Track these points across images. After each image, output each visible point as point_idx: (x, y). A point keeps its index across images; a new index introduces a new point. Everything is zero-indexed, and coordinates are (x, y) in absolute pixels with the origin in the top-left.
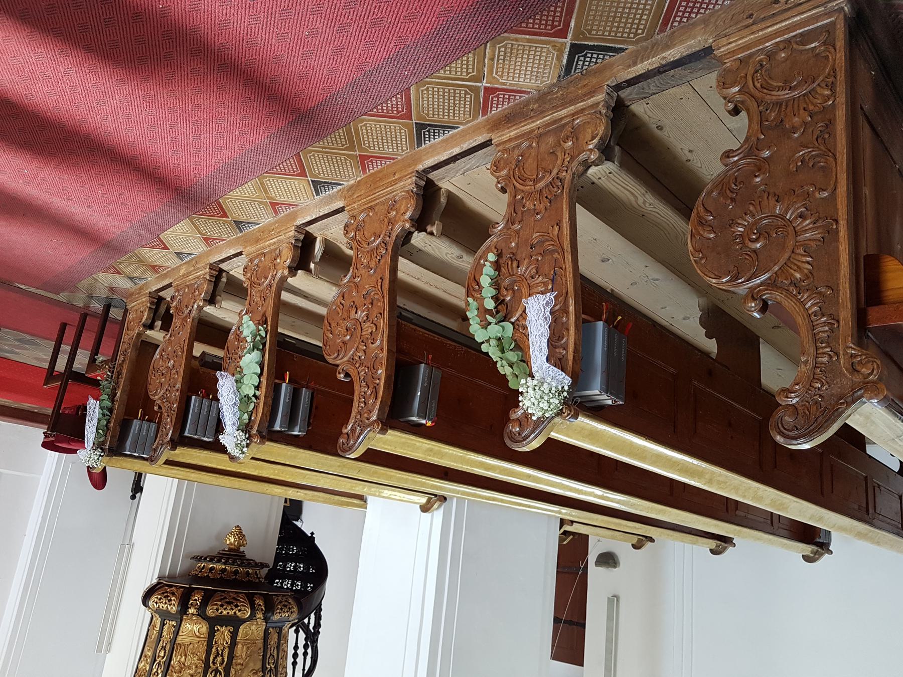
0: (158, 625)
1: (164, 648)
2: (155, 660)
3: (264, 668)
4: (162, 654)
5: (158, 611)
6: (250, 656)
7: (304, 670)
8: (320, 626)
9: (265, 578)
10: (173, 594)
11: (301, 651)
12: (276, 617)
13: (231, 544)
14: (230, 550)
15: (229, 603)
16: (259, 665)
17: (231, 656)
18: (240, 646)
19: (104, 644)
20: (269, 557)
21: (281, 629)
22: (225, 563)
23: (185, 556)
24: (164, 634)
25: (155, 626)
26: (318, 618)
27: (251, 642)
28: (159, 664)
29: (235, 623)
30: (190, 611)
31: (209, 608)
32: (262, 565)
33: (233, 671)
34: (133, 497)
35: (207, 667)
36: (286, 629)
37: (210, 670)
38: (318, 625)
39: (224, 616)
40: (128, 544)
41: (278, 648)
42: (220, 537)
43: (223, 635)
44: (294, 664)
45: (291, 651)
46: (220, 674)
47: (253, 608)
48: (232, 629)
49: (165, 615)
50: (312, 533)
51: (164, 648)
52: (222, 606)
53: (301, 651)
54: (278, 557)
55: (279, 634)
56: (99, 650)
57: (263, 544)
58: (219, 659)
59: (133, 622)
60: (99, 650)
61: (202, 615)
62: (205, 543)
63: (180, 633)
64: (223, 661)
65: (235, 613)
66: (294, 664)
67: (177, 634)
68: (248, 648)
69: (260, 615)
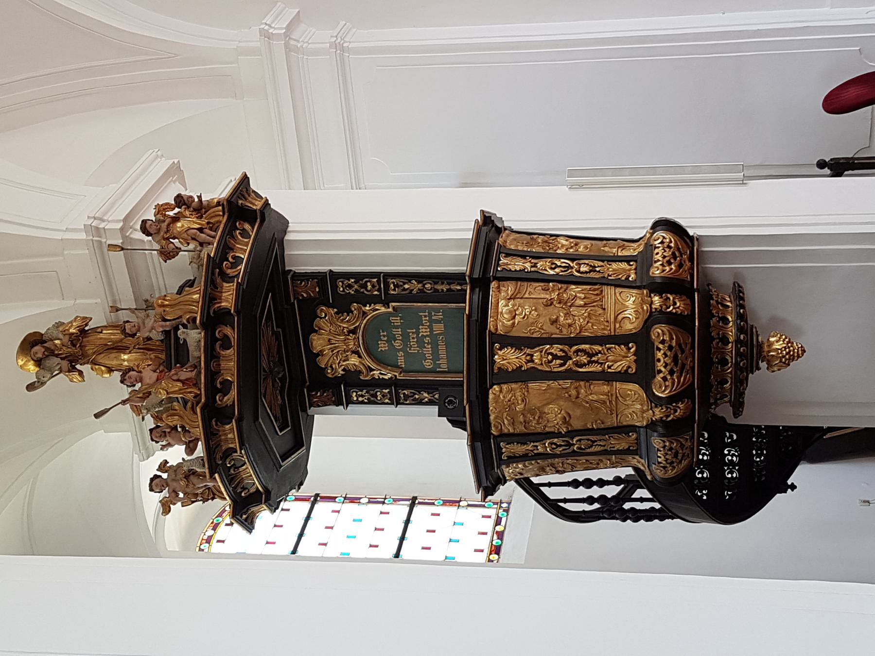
0: (626, 253)
1: (593, 269)
2: (573, 260)
3: (572, 433)
4: (584, 268)
5: (649, 248)
6: (591, 408)
7: (565, 501)
8: (636, 520)
9: (715, 416)
10: (680, 266)
11: (596, 492)
12: (657, 442)
13: (770, 344)
14: (760, 346)
15: (675, 359)
16: (577, 425)
17: (590, 377)
18: (606, 388)
19: (581, 178)
20: (751, 416)
21: (635, 453)
22: (738, 341)
23: (736, 273)
24: (615, 266)
25: (623, 248)
26: (649, 516)
27: (614, 403)
28: (569, 267)
29: (643, 374)
30: (656, 299)
31: (665, 328)
32: (738, 407)
33: (567, 383)
34: (821, 164)
35: (570, 342)
36: (634, 462)
37: (566, 348)
38: (636, 516)
39: (653, 355)
40: (749, 174)
41: (605, 452)
42: (777, 324)
43: (622, 359)
44: (575, 484)
45: (594, 475)
46: (561, 365)
47: (671, 400)
48: (633, 370)
49: (644, 260)
50: (793, 487)
51: (593, 269)
52: (670, 348)
53: (596, 492)
54: (746, 431)
55: (628, 452)
56: (571, 173)
57: (778, 398)
58: (584, 359)
59: (621, 214)
60: (571, 173)
61: (652, 319)
62: (762, 302)
63: (618, 290)
64: (582, 366)
65: (660, 371)
66: (575, 484)
67: (616, 286)
68: (604, 402)
69: (658, 413)
